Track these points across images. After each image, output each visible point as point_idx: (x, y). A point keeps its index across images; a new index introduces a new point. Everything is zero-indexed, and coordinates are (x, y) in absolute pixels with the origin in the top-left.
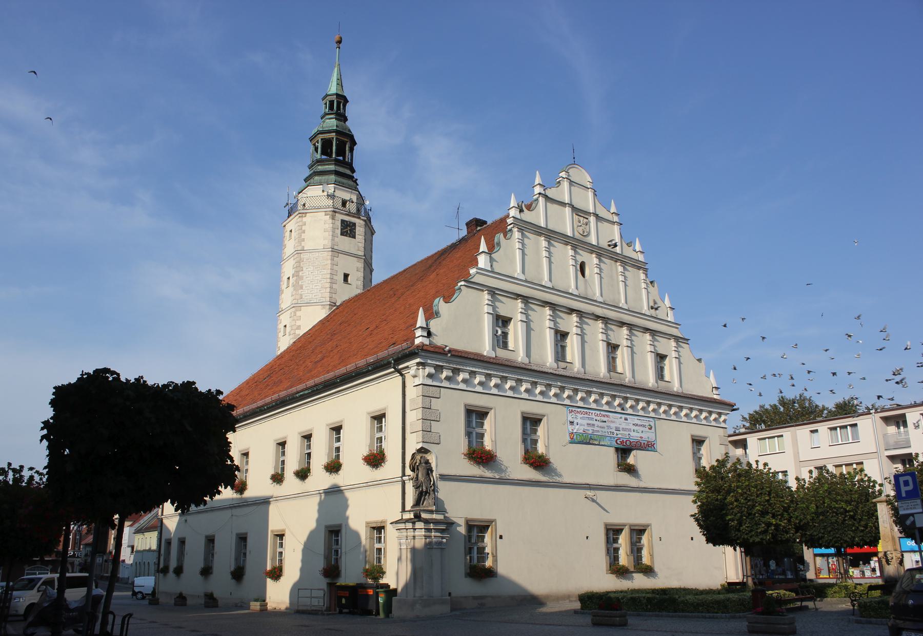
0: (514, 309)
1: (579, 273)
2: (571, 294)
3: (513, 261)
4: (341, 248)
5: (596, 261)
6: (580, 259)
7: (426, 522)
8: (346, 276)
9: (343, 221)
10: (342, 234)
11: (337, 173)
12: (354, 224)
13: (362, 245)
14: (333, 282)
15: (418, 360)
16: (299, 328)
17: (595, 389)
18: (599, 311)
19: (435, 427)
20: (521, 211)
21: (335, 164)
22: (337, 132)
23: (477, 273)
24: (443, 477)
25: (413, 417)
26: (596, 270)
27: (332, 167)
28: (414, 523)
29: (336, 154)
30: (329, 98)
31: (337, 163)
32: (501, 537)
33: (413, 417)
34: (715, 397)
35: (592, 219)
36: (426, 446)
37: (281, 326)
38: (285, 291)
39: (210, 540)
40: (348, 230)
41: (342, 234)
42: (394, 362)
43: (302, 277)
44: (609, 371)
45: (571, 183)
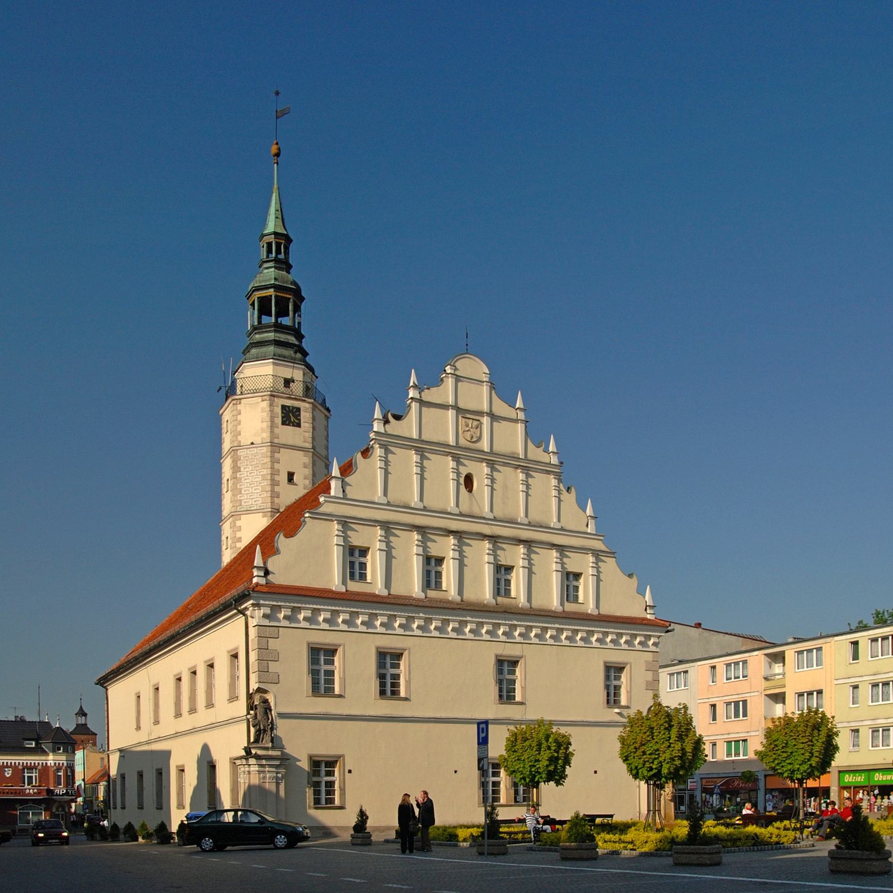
0: (373, 539)
1: (462, 488)
2: (450, 514)
3: (373, 485)
4: (282, 440)
5: (486, 470)
6: (464, 471)
7: (257, 757)
8: (291, 476)
9: (283, 407)
10: (283, 423)
11: (278, 343)
12: (299, 410)
13: (309, 435)
14: (274, 483)
15: (251, 602)
16: (240, 540)
17: (469, 618)
18: (487, 530)
19: (273, 667)
20: (386, 422)
21: (275, 331)
22: (276, 287)
23: (326, 501)
24: (282, 716)
25: (253, 656)
26: (487, 482)
27: (271, 336)
28: (247, 759)
29: (281, 317)
30: (267, 239)
31: (278, 327)
32: (350, 771)
33: (253, 656)
34: (649, 617)
35: (486, 420)
36: (263, 686)
37: (224, 538)
38: (226, 495)
39: (141, 775)
40: (290, 417)
41: (283, 423)
42: (234, 605)
43: (241, 479)
44: (497, 592)
45: (458, 379)
